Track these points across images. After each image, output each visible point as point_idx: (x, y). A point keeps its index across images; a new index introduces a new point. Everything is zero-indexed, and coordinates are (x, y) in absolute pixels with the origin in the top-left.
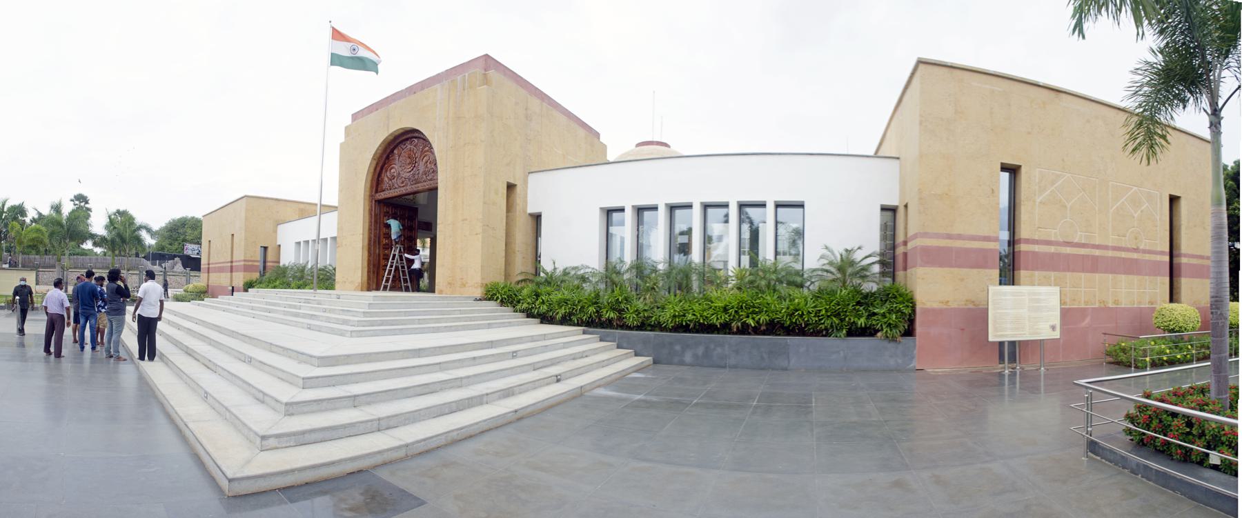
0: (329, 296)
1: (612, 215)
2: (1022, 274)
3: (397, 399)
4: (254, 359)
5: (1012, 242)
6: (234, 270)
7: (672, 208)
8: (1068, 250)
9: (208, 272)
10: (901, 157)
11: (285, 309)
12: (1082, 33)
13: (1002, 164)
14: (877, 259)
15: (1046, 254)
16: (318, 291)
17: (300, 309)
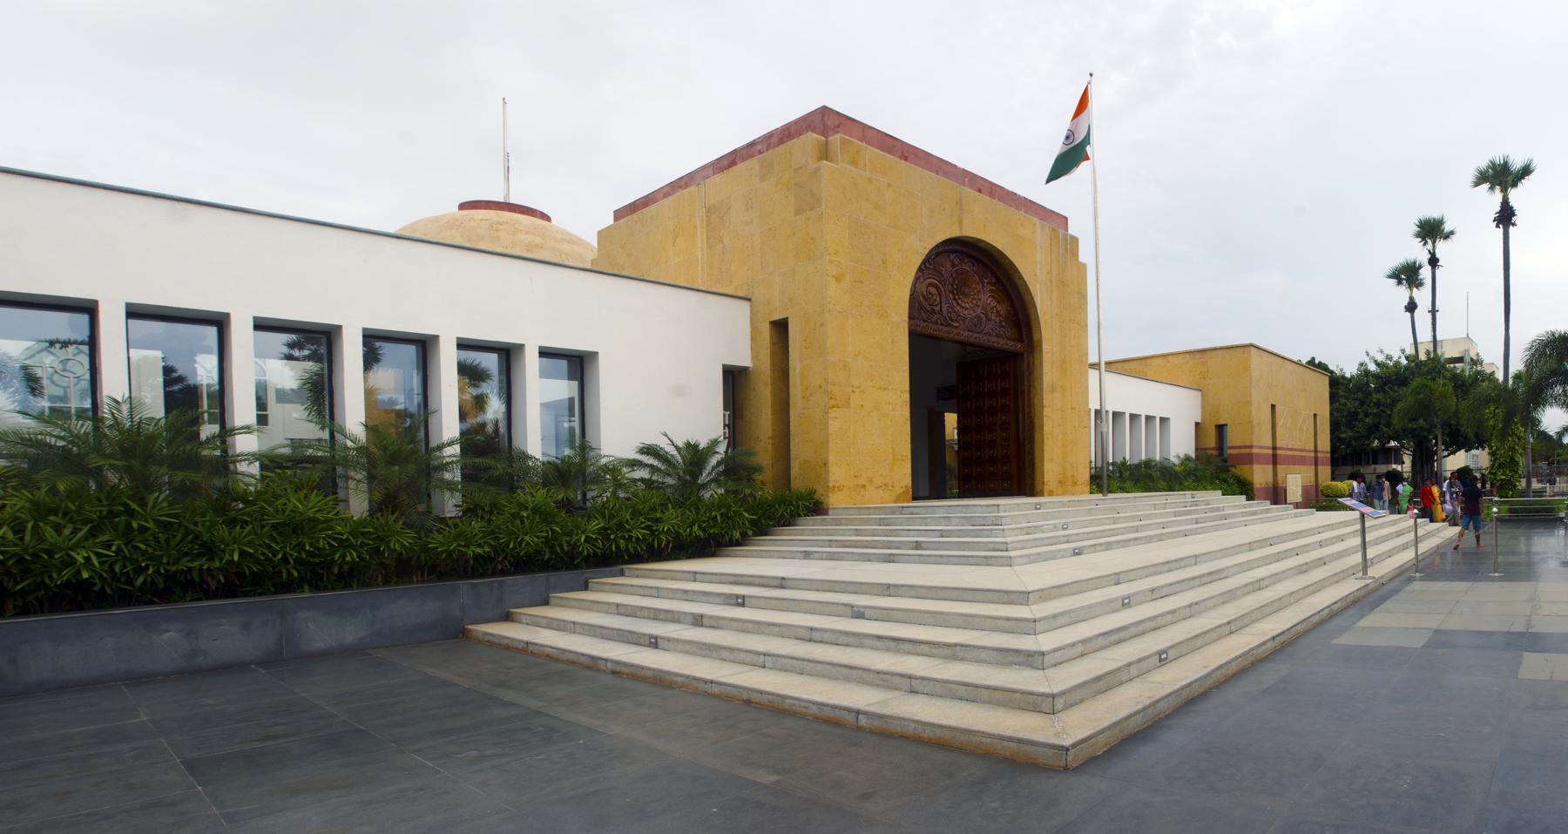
4: (663, 638)
5: (1274, 448)
6: (1319, 463)
9: (1316, 465)
11: (1207, 515)
12: (1452, 233)
13: (128, 305)
14: (763, 452)
15: (1285, 455)
16: (1111, 496)
17: (1223, 510)
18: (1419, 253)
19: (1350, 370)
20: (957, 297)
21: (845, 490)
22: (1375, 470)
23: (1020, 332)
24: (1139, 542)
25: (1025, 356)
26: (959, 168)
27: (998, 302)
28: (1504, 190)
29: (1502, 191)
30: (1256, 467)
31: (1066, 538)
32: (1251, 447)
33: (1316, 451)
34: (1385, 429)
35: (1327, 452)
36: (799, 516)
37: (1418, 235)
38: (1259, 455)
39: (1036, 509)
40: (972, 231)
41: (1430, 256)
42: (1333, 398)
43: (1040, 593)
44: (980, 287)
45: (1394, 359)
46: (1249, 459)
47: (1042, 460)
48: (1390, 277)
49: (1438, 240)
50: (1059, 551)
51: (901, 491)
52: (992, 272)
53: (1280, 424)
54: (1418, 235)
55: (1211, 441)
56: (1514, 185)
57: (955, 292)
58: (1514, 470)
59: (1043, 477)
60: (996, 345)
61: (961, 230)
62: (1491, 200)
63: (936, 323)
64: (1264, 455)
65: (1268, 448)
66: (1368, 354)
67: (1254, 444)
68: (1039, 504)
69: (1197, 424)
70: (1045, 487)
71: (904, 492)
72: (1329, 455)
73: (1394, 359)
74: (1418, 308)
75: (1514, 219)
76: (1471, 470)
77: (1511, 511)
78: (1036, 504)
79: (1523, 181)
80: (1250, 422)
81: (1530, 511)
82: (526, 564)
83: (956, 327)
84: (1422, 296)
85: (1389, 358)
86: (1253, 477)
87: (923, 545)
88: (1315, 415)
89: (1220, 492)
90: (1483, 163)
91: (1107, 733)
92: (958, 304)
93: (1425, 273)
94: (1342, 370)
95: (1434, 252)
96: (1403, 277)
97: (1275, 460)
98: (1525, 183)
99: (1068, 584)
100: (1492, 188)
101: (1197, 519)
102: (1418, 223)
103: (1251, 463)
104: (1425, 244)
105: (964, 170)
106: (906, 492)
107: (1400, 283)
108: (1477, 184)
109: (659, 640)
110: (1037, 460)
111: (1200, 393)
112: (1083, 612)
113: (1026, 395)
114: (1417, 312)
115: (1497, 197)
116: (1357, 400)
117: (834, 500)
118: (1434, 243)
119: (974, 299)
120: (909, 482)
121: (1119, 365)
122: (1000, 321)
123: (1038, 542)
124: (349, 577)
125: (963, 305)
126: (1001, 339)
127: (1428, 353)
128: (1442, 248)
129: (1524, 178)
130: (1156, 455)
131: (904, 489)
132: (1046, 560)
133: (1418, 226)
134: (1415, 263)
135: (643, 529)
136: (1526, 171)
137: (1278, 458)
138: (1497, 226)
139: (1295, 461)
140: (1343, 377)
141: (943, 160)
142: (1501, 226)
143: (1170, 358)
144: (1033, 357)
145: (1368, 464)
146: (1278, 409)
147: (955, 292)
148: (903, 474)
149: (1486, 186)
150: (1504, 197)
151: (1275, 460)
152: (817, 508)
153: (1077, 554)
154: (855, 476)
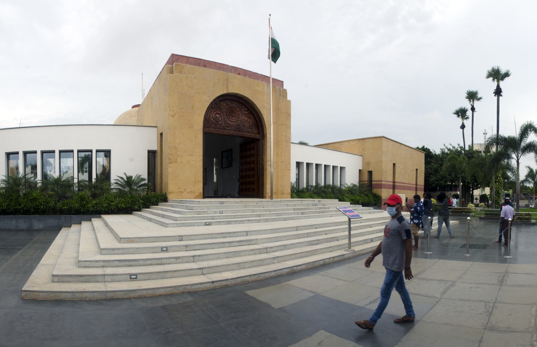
0: (313, 201)
1: (26, 155)
2: (422, 192)
3: (235, 256)
5: (394, 182)
7: (25, 153)
8: (401, 184)
10: (158, 126)
12: (481, 98)
17: (329, 209)
18: (467, 104)
19: (438, 152)
20: (229, 117)
21: (175, 193)
22: (451, 193)
23: (259, 130)
24: (249, 222)
25: (261, 140)
26: (230, 66)
27: (248, 118)
28: (498, 81)
29: (497, 81)
30: (383, 190)
31: (212, 217)
32: (381, 181)
33: (416, 185)
34: (448, 177)
35: (422, 186)
36: (159, 202)
37: (467, 98)
38: (385, 184)
39: (221, 204)
40: (233, 89)
41: (471, 107)
42: (427, 163)
43: (127, 239)
44: (240, 113)
45: (456, 148)
46: (380, 186)
47: (266, 184)
48: (455, 114)
49: (475, 101)
50: (196, 223)
51: (198, 194)
52: (245, 106)
53: (398, 172)
54: (467, 98)
55: (366, 177)
56: (502, 79)
57: (228, 115)
58: (499, 196)
59: (266, 190)
60: (246, 136)
61: (228, 90)
62: (492, 85)
63: (219, 128)
64: (388, 185)
65: (391, 182)
66: (445, 145)
67: (383, 180)
68: (223, 202)
69: (360, 170)
70: (267, 195)
71: (199, 195)
72: (423, 187)
73: (456, 148)
74: (466, 127)
75: (501, 93)
76: (487, 195)
77: (486, 214)
78: (221, 202)
79: (505, 78)
80: (382, 170)
81: (493, 215)
82: (78, 212)
83: (228, 130)
84: (468, 123)
85: (454, 147)
86: (381, 195)
87: (164, 216)
88: (417, 170)
89: (338, 200)
90: (490, 69)
91: (45, 294)
92: (229, 120)
93: (469, 113)
94: (435, 151)
95: (473, 105)
96: (460, 114)
97: (394, 187)
98: (506, 79)
99: (146, 237)
100: (494, 80)
101: (302, 212)
102: (467, 93)
103: (381, 188)
104: (470, 102)
105: (232, 66)
106: (201, 195)
107: (458, 116)
108: (488, 77)
109: (168, 248)
110: (265, 183)
111: (361, 157)
112: (132, 250)
113: (261, 156)
114: (465, 129)
115: (495, 83)
116: (439, 164)
117: (170, 197)
118: (473, 101)
119: (236, 118)
120: (201, 191)
121: (324, 146)
122: (250, 126)
123: (240, 217)
124: (43, 212)
125: (232, 120)
126: (252, 134)
127: (469, 146)
128: (476, 104)
129: (506, 77)
130: (330, 182)
131: (199, 194)
132: (187, 226)
133: (467, 94)
134: (465, 108)
135: (107, 204)
136: (507, 75)
137: (396, 187)
138: (495, 96)
139: (404, 188)
140: (435, 155)
141: (222, 64)
142: (496, 95)
143: (351, 142)
144: (264, 141)
145: (448, 191)
146: (397, 166)
147: (228, 115)
148: (199, 187)
149: (491, 79)
150: (498, 84)
151: (394, 187)
152: (165, 199)
153: (207, 225)
154: (179, 188)
